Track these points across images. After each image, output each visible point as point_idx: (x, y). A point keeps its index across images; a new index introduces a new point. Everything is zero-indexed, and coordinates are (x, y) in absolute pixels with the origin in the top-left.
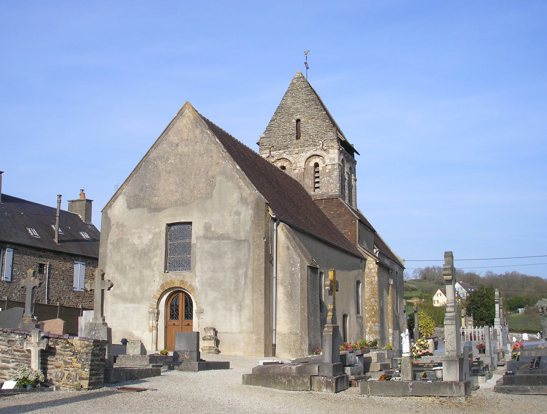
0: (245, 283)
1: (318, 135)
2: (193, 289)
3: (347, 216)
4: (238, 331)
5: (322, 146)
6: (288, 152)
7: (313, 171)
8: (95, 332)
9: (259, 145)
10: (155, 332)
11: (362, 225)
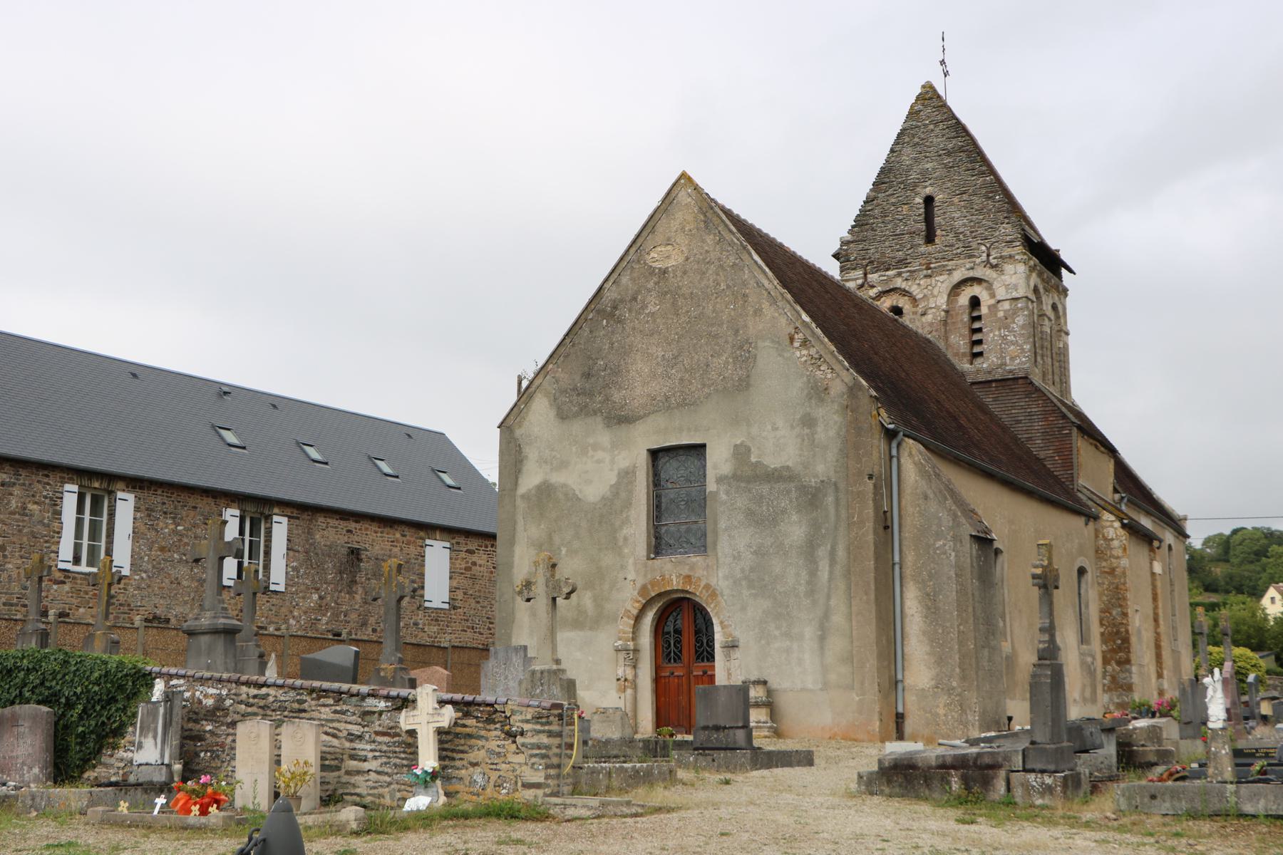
0: (830, 580)
2: (714, 595)
3: (1051, 419)
4: (820, 686)
6: (908, 274)
9: (838, 259)
10: (629, 691)
11: (1086, 437)
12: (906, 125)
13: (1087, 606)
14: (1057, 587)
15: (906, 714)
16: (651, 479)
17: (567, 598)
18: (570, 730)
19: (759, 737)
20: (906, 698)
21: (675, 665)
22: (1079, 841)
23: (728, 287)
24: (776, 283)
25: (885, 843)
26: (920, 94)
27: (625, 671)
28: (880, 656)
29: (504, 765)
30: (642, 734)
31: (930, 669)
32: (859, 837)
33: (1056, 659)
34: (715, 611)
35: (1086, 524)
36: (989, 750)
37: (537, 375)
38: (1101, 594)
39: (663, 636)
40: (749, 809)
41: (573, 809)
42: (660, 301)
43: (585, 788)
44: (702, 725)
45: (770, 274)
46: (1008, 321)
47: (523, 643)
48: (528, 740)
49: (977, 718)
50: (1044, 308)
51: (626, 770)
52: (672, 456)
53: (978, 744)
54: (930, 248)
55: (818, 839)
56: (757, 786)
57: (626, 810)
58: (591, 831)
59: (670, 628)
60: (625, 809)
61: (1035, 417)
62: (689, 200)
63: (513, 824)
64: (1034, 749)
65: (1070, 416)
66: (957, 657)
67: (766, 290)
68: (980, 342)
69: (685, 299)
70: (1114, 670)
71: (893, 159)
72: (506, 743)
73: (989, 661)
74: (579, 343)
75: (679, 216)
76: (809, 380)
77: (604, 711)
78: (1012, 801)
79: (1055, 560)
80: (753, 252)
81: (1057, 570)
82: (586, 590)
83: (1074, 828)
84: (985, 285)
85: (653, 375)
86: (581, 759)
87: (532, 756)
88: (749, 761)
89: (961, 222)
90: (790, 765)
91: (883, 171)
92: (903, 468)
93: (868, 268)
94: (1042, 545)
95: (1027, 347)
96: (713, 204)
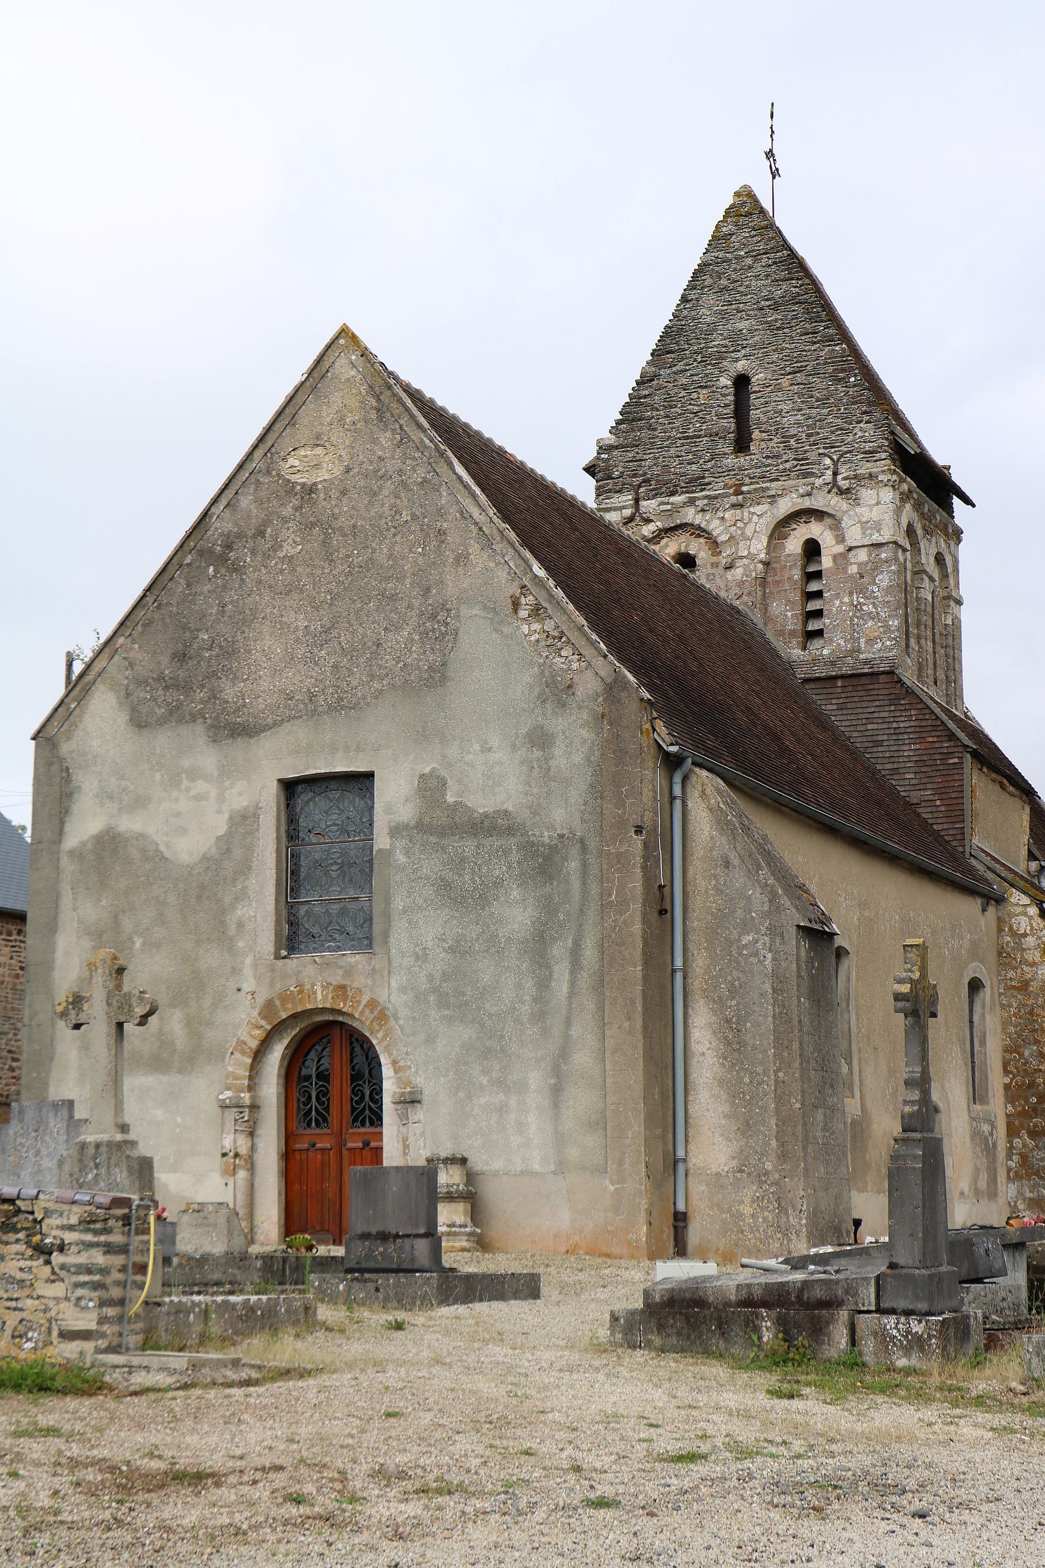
0: (571, 995)
1: (818, 434)
2: (382, 1017)
3: (930, 739)
4: (552, 1167)
5: (831, 477)
6: (706, 501)
7: (799, 572)
8: (95, 1172)
9: (593, 475)
10: (242, 1174)
11: (985, 770)
12: (710, 257)
13: (983, 1043)
14: (934, 1015)
15: (689, 1214)
16: (283, 828)
17: (139, 1024)
18: (142, 1242)
19: (452, 1250)
20: (690, 1189)
21: (318, 1131)
22: (966, 1430)
23: (414, 517)
24: (491, 514)
25: (652, 1430)
26: (731, 207)
27: (235, 1140)
28: (650, 1120)
29: (29, 1302)
30: (262, 1244)
31: (729, 1140)
32: (610, 1419)
33: (931, 1130)
34: (385, 1044)
35: (984, 910)
36: (822, 1276)
37: (98, 654)
38: (1005, 1024)
39: (299, 1083)
40: (434, 1372)
41: (143, 1373)
42: (303, 538)
43: (164, 1337)
44: (359, 1232)
45: (482, 497)
47: (68, 1095)
48: (71, 1259)
49: (804, 1221)
50: (924, 561)
51: (233, 1306)
52: (317, 790)
53: (804, 1267)
54: (743, 460)
55: (545, 1423)
56: (447, 1333)
57: (231, 1375)
58: (172, 1410)
59: (311, 1069)
60: (229, 1373)
61: (905, 736)
62: (353, 373)
63: (41, 1401)
64: (894, 1276)
65: (961, 735)
66: (773, 1121)
67: (476, 524)
68: (818, 614)
69: (344, 535)
70: (1024, 1145)
71: (685, 312)
72: (35, 1263)
73: (825, 1129)
74: (169, 604)
75: (336, 398)
76: (542, 673)
77: (200, 1209)
78: (859, 1361)
79: (931, 966)
80: (455, 462)
81: (935, 986)
82: (175, 1007)
83: (957, 1406)
84: (828, 521)
85: (290, 659)
86: (159, 1289)
87: (77, 1285)
88: (434, 1290)
89: (792, 419)
90: (502, 1297)
91: (669, 333)
92: (691, 817)
93: (642, 490)
94: (911, 946)
95: (894, 623)
96: (392, 382)
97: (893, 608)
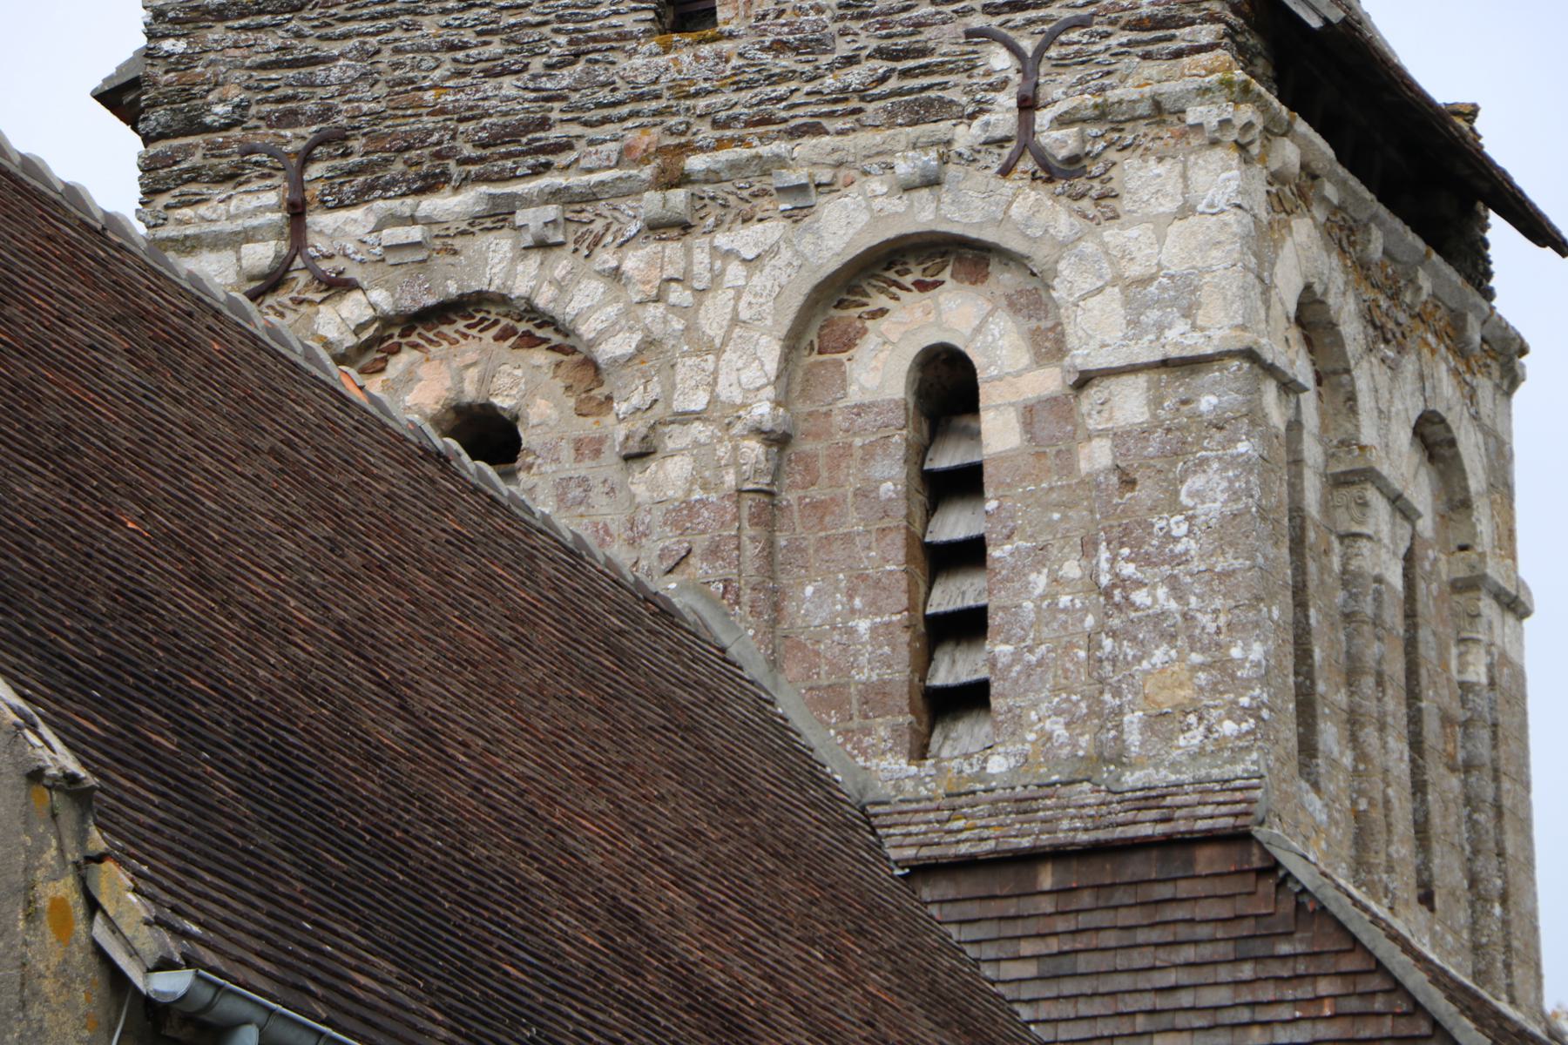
6: (552, 211)
46: (1144, 493)
50: (1368, 435)
84: (1004, 279)
93: (315, 170)
95: (1250, 652)
97: (1244, 596)
